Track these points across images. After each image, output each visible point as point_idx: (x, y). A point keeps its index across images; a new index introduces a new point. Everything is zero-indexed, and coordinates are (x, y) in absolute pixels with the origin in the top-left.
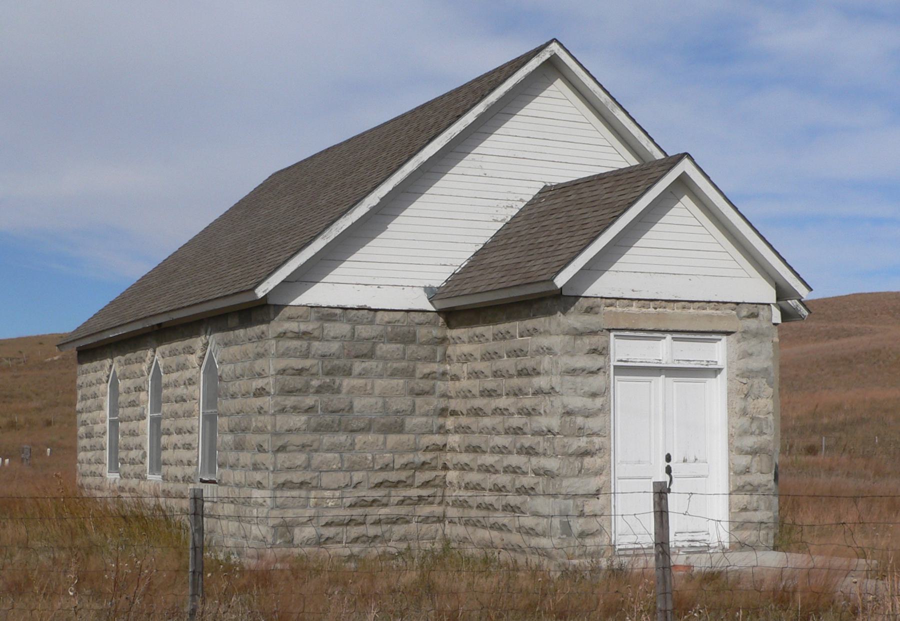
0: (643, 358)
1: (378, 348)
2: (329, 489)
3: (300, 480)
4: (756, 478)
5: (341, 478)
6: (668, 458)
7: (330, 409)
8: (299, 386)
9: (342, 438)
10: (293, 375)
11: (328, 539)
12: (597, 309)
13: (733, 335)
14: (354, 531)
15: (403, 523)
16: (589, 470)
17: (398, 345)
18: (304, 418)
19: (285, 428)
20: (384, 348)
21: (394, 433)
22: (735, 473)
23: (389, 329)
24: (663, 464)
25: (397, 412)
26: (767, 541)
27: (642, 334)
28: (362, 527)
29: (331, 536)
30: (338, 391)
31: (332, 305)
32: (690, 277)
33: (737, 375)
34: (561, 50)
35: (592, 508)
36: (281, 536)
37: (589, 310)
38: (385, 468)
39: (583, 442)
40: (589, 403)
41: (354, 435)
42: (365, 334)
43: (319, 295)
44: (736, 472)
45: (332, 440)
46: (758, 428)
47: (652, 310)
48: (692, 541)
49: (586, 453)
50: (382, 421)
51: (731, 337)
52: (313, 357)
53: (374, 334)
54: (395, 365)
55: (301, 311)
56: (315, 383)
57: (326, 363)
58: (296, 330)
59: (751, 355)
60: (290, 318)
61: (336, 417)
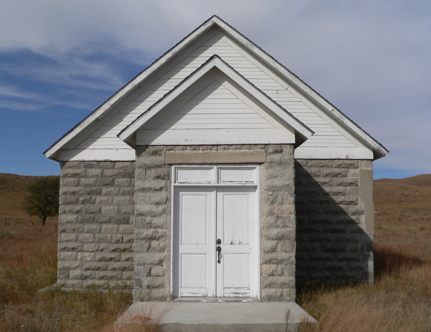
0: (197, 181)
1: (116, 181)
2: (87, 252)
3: (72, 247)
4: (280, 255)
5: (93, 246)
6: (219, 242)
7: (89, 212)
8: (73, 200)
9: (94, 226)
10: (71, 195)
11: (86, 277)
12: (160, 152)
13: (263, 165)
14: (101, 273)
15: (128, 270)
16: (155, 248)
17: (127, 179)
18: (75, 216)
19: (65, 221)
20: (119, 181)
21: (124, 224)
22: (265, 252)
23: (122, 171)
24: (213, 246)
25: (125, 213)
26: (290, 295)
27: (195, 166)
28: (105, 272)
29: (88, 275)
30: (94, 202)
31: (91, 160)
32: (228, 130)
33: (266, 190)
34: (219, 21)
35: (156, 272)
36: (63, 274)
37: (155, 153)
38: (118, 242)
39: (150, 232)
40: (154, 208)
41: (102, 224)
42: (108, 174)
43: (85, 155)
44: (264, 251)
45: (89, 227)
46: (282, 223)
47: (201, 151)
48: (237, 293)
49: (153, 238)
50: (117, 218)
51: (262, 166)
52: (81, 186)
53: (114, 174)
54: (125, 189)
55: (75, 164)
56: (82, 199)
57: (88, 189)
58: (72, 173)
59: (276, 176)
60: (70, 167)
61: (92, 216)
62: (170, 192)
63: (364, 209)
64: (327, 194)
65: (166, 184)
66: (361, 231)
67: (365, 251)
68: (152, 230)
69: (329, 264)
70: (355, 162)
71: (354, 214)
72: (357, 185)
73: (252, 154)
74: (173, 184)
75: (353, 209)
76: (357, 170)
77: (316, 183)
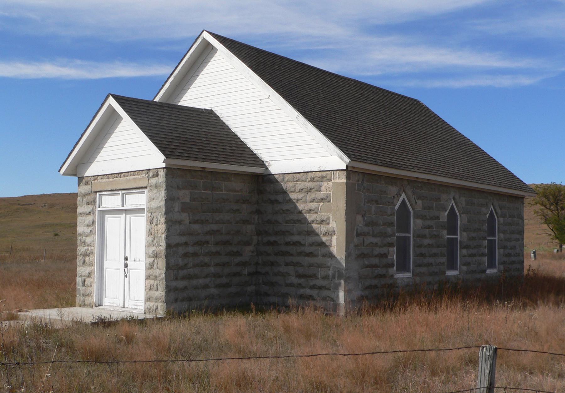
6: (126, 259)
48: (136, 305)
62: (95, 215)
63: (335, 229)
64: (300, 212)
65: (93, 209)
66: (331, 256)
67: (336, 279)
68: (86, 248)
69: (302, 291)
70: (327, 174)
71: (325, 234)
72: (330, 201)
73: (139, 179)
74: (98, 209)
75: (324, 229)
76: (331, 184)
77: (290, 200)
